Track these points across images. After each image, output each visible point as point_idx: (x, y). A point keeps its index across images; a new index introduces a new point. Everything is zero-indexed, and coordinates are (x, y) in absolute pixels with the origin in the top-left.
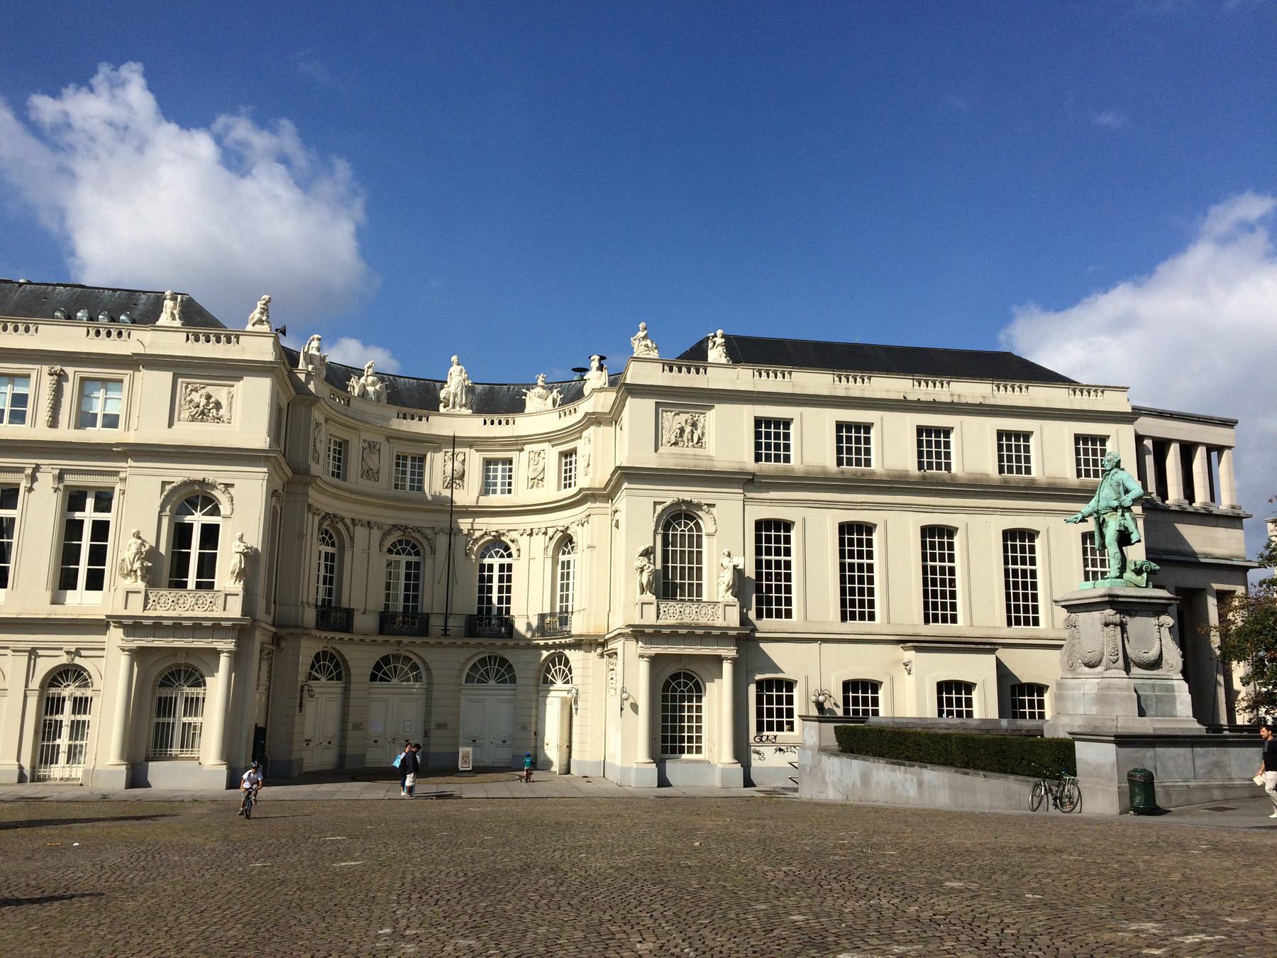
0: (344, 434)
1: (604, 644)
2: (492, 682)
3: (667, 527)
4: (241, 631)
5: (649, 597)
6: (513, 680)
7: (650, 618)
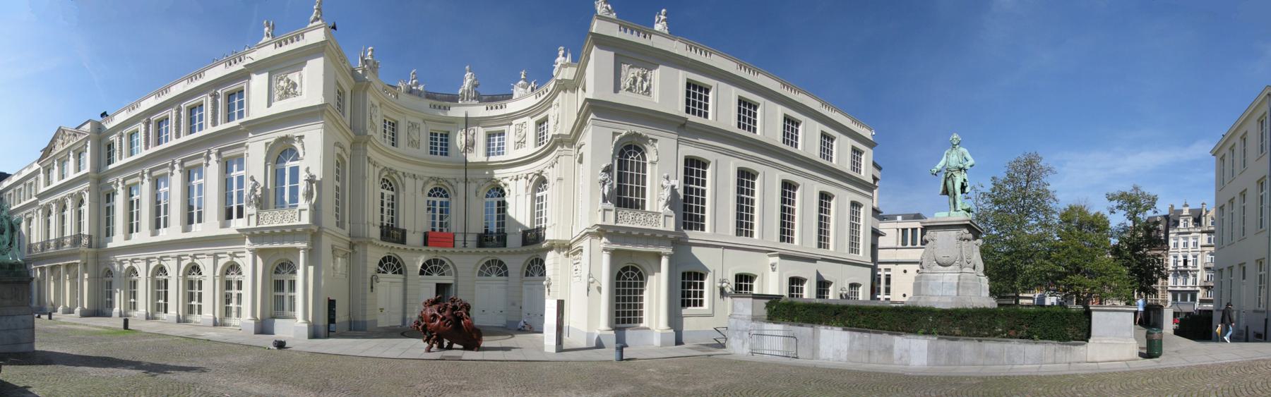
0: (394, 116)
1: (569, 247)
2: (494, 276)
3: (621, 153)
4: (313, 234)
5: (609, 205)
6: (506, 274)
7: (610, 221)
